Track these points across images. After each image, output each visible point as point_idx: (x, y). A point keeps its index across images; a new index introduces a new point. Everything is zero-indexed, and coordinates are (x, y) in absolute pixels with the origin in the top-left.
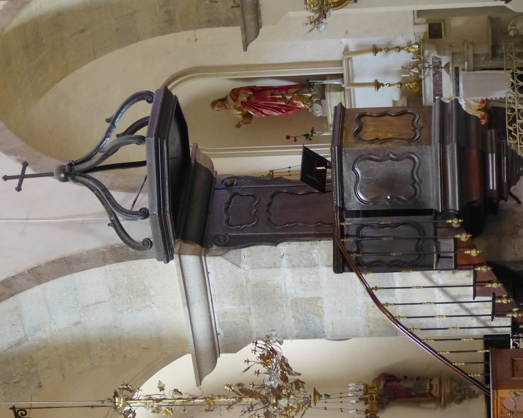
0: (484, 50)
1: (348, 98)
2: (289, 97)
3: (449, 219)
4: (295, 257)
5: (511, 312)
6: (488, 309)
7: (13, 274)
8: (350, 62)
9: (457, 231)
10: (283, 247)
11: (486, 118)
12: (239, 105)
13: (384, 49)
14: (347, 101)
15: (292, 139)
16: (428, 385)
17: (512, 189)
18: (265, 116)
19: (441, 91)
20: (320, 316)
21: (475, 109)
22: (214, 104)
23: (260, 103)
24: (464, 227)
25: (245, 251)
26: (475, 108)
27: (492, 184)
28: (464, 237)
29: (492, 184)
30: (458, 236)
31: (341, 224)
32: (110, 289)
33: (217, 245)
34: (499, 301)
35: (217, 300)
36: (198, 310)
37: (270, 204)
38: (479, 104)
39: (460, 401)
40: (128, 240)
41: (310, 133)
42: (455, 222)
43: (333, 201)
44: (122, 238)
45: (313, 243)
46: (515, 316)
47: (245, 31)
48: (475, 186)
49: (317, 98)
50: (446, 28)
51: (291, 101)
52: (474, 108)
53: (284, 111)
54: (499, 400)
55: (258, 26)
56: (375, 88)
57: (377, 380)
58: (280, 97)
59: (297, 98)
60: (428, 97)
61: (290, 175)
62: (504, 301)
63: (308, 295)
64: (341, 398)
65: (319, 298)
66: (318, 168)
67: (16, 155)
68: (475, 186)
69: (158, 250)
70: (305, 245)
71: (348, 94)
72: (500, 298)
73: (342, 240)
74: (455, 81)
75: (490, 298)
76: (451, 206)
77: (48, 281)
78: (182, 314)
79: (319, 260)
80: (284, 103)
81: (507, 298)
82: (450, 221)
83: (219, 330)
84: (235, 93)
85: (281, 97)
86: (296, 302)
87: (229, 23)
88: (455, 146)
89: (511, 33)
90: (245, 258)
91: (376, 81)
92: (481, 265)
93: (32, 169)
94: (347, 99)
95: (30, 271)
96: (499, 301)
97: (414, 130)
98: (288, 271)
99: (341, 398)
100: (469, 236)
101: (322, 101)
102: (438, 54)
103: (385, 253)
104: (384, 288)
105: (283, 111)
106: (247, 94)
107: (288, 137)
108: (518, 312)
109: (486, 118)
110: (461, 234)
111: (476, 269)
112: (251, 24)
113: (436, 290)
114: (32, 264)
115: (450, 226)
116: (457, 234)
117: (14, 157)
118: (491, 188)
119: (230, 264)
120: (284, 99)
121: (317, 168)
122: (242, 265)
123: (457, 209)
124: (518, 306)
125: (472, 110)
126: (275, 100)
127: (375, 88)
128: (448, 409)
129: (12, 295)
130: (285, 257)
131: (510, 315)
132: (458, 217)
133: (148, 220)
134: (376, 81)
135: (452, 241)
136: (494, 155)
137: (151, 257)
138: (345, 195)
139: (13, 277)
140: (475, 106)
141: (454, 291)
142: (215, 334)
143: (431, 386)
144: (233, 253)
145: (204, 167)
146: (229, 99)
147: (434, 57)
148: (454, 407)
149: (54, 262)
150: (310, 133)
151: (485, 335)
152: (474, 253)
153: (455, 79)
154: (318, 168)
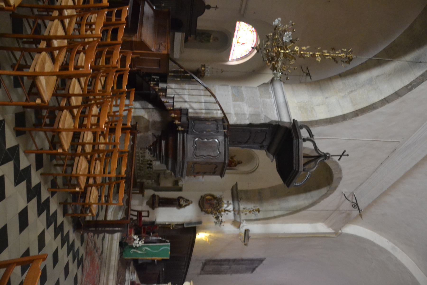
0: (162, 176)
3: (183, 130)
5: (159, 89)
6: (169, 91)
9: (179, 125)
10: (247, 122)
17: (155, 139)
20: (233, 94)
22: (242, 162)
24: (176, 126)
25: (262, 122)
27: (163, 143)
28: (177, 122)
29: (163, 143)
30: (179, 123)
32: (314, 110)
34: (164, 94)
35: (273, 103)
36: (281, 100)
37: (249, 139)
40: (308, 129)
42: (180, 128)
43: (229, 140)
44: (310, 130)
45: (236, 123)
46: (157, 87)
47: (237, 189)
48: (170, 143)
54: (167, 49)
55: (232, 189)
62: (161, 94)
63: (238, 103)
65: (233, 101)
68: (170, 143)
69: (298, 125)
70: (239, 122)
72: (163, 95)
75: (168, 95)
76: (181, 135)
77: (341, 116)
78: (288, 99)
79: (234, 117)
81: (160, 95)
82: (182, 129)
83: (271, 92)
84: (235, 165)
86: (242, 100)
87: (241, 191)
88: (178, 160)
89: (153, 181)
92: (171, 110)
96: (164, 94)
98: (246, 112)
100: (175, 122)
103: (6, 86)
108: (156, 89)
110: (178, 124)
112: (235, 190)
113: (188, 101)
115: (182, 127)
116: (180, 124)
118: (164, 141)
119: (269, 117)
122: (264, 116)
123: (178, 134)
124: (156, 92)
129: (356, 111)
131: (159, 88)
132: (179, 131)
133: (303, 138)
135: (182, 121)
136: (162, 154)
137: (299, 122)
138: (224, 142)
141: (181, 100)
142: (273, 90)
144: (267, 121)
146: (237, 164)
152: (173, 115)
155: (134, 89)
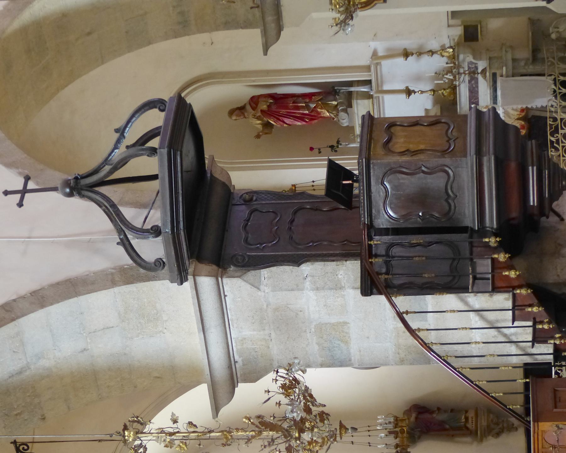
0: (524, 54)
1: (377, 106)
2: (313, 106)
3: (486, 238)
4: (319, 279)
5: (553, 338)
6: (528, 335)
7: (14, 297)
8: (378, 67)
9: (495, 250)
10: (307, 268)
11: (526, 128)
12: (259, 114)
13: (416, 53)
14: (376, 110)
15: (316, 151)
16: (463, 417)
17: (554, 205)
18: (287, 126)
19: (478, 98)
20: (347, 343)
21: (514, 118)
22: (231, 113)
23: (281, 112)
24: (503, 247)
25: (265, 272)
26: (514, 117)
27: (533, 200)
28: (502, 257)
29: (533, 200)
30: (496, 256)
31: (369, 243)
32: (119, 314)
33: (235, 265)
34: (540, 327)
35: (235, 326)
36: (214, 336)
37: (292, 221)
38: (519, 113)
39: (498, 435)
40: (139, 260)
41: (335, 144)
42: (493, 241)
43: (360, 218)
44: (132, 258)
45: (338, 263)
46: (558, 342)
47: (265, 33)
48: (514, 201)
49: (343, 106)
50: (482, 30)
51: (315, 109)
52: (513, 117)
53: (308, 121)
54: (540, 434)
55: (280, 29)
56: (405, 95)
57: (408, 412)
58: (302, 105)
59: (321, 106)
60: (463, 105)
61: (314, 190)
62: (546, 327)
63: (334, 320)
64: (369, 431)
65: (345, 323)
66: (344, 182)
67: (17, 168)
68: (514, 201)
69: (171, 271)
70: (330, 266)
71: (377, 102)
72: (542, 322)
73: (370, 261)
74: (493, 88)
75: (530, 323)
76: (488, 223)
77: (52, 304)
78: (197, 340)
79: (345, 281)
80: (307, 112)
81: (549, 323)
82: (487, 240)
83: (237, 358)
84: (254, 101)
85: (304, 105)
86: (321, 328)
87: (247, 25)
88: (493, 158)
89: (553, 36)
90: (265, 279)
91: (407, 87)
92: (520, 287)
93: (35, 183)
94: (376, 107)
95: (33, 294)
96: (540, 327)
97: (448, 141)
98: (311, 294)
99: (369, 431)
100: (507, 256)
101: (349, 109)
102: (474, 58)
103: (417, 274)
104: (415, 312)
105: (306, 120)
106: (267, 102)
107: (312, 149)
108: (561, 338)
109: (526, 128)
110: (499, 253)
111: (515, 292)
112: (272, 26)
113: (472, 314)
114: (34, 287)
115: (487, 245)
116: (494, 253)
117: (15, 170)
118: (532, 204)
119: (249, 286)
120: (307, 107)
121: (343, 182)
122: (262, 287)
123: (495, 226)
124: (561, 332)
125: (511, 120)
126: (298, 108)
127: (406, 96)
128: (485, 443)
129: (13, 320)
130: (309, 279)
131: (552, 342)
132: (496, 235)
133: (160, 238)
134: (407, 87)
135: (489, 261)
136: (535, 168)
137: (164, 279)
138: (374, 211)
139: (14, 300)
140: (514, 115)
141: (491, 316)
142: (233, 362)
143: (467, 419)
144: (252, 274)
145: (221, 181)
146: (248, 107)
147: (470, 62)
148: (491, 441)
149: (58, 284)
150: (335, 144)
151: (524, 363)
152: (513, 274)
153: (493, 86)
154: (344, 182)
155: (510, 255)
